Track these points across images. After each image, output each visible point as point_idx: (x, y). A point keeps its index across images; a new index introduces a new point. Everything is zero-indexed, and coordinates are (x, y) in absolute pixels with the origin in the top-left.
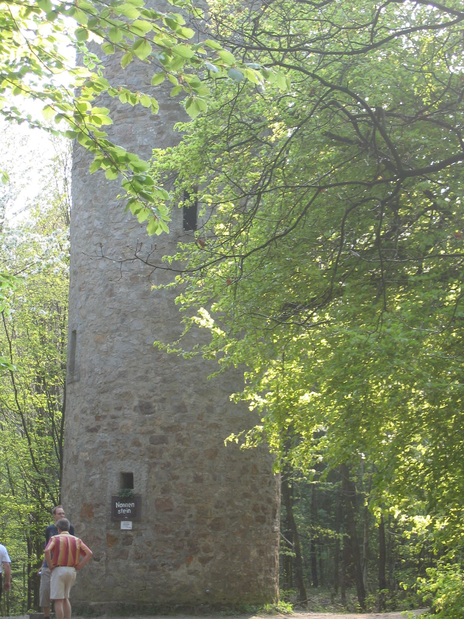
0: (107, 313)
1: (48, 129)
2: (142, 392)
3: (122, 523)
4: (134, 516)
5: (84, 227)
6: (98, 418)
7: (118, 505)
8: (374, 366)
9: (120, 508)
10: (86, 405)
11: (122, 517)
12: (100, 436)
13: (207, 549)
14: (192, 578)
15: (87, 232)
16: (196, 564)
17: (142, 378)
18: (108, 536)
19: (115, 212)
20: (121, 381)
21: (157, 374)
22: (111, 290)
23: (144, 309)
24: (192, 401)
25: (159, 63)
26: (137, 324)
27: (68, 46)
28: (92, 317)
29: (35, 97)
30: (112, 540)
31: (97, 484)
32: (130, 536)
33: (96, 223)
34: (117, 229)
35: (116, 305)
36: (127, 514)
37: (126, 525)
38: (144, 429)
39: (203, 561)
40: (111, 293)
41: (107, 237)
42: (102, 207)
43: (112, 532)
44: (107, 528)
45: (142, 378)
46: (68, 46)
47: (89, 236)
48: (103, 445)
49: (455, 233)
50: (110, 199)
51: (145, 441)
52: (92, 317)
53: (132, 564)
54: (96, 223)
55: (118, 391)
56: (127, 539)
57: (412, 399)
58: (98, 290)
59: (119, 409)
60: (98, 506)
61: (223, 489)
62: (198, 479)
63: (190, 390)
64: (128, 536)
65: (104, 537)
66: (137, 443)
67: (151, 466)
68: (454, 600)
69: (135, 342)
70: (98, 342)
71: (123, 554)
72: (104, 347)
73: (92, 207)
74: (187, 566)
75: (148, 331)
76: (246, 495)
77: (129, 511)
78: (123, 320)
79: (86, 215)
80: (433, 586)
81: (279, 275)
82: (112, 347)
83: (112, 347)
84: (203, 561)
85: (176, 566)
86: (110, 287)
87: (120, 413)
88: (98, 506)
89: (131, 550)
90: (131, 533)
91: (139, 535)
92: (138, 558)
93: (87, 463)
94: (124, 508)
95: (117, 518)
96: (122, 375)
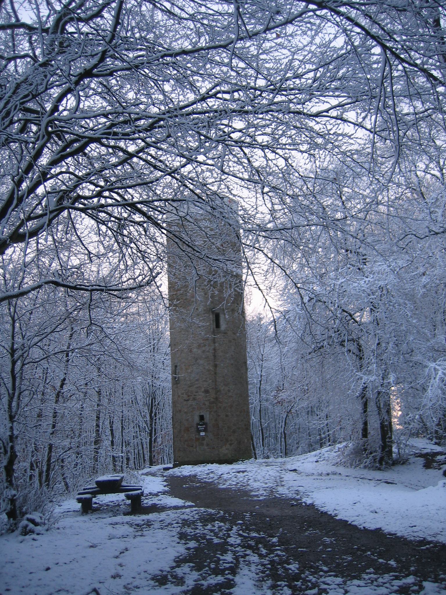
0: (190, 359)
2: (205, 386)
4: (205, 430)
6: (188, 396)
7: (199, 427)
8: (178, 175)
10: (183, 392)
11: (201, 431)
12: (190, 402)
13: (231, 441)
14: (227, 451)
16: (228, 446)
17: (204, 381)
18: (196, 438)
20: (196, 382)
21: (210, 379)
23: (204, 356)
24: (223, 388)
26: (201, 362)
31: (190, 420)
35: (193, 355)
37: (203, 434)
38: (207, 399)
39: (231, 444)
40: (191, 351)
41: (188, 332)
43: (197, 436)
44: (195, 435)
45: (204, 381)
47: (180, 332)
48: (191, 405)
51: (207, 403)
55: (196, 386)
56: (203, 438)
58: (186, 351)
59: (197, 392)
60: (191, 427)
61: (235, 419)
62: (227, 416)
63: (222, 384)
64: (203, 438)
65: (194, 438)
66: (204, 404)
67: (210, 412)
70: (186, 369)
71: (202, 444)
72: (189, 371)
75: (206, 364)
76: (242, 421)
78: (196, 361)
84: (231, 444)
87: (197, 394)
88: (191, 427)
89: (205, 442)
91: (207, 437)
92: (208, 445)
93: (186, 412)
95: (199, 431)
96: (197, 380)
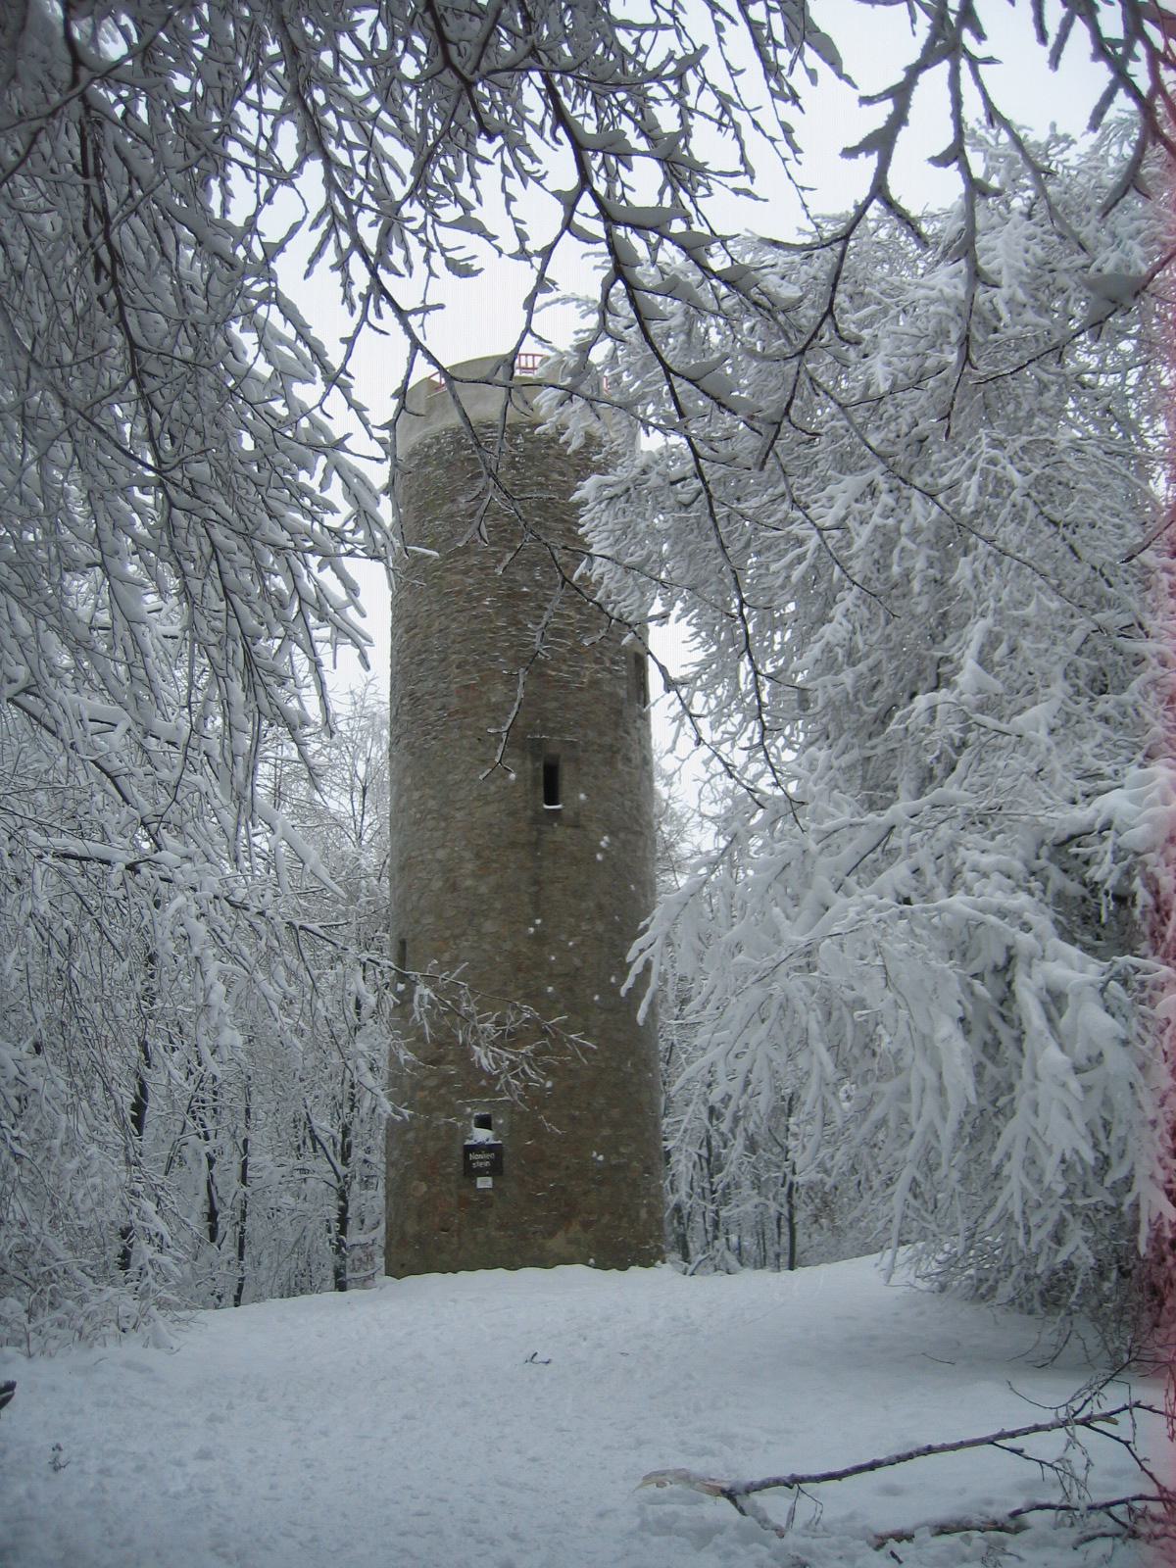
0: (451, 913)
1: (724, 406)
3: (479, 1179)
22: (454, 884)
27: (742, 71)
28: (429, 920)
29: (149, 1370)
30: (464, 1202)
33: (432, 804)
36: (487, 1168)
37: (484, 1183)
40: (454, 887)
46: (742, 71)
52: (429, 920)
54: (432, 804)
57: (369, 744)
74: (566, 1232)
77: (487, 1164)
80: (56, 410)
85: (552, 1234)
90: (491, 1193)
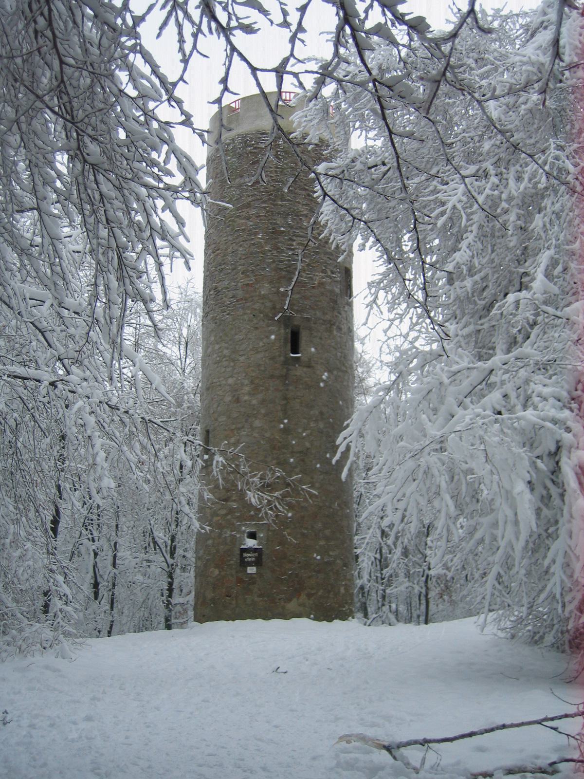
5: (216, 355)
9: (246, 557)
15: (218, 359)
19: (240, 343)
25: (217, 30)
32: (254, 578)
33: (226, 352)
34: (241, 356)
36: (253, 562)
39: (309, 596)
40: (238, 400)
42: (230, 340)
43: (240, 575)
44: (237, 572)
49: (281, 430)
50: (236, 334)
53: (256, 599)
68: (62, 155)
69: (256, 435)
73: (222, 341)
77: (253, 559)
79: (217, 347)
81: (456, 306)
82: (239, 440)
83: (239, 440)
86: (236, 397)
90: (255, 576)
94: (250, 557)
